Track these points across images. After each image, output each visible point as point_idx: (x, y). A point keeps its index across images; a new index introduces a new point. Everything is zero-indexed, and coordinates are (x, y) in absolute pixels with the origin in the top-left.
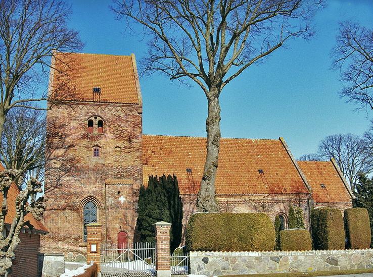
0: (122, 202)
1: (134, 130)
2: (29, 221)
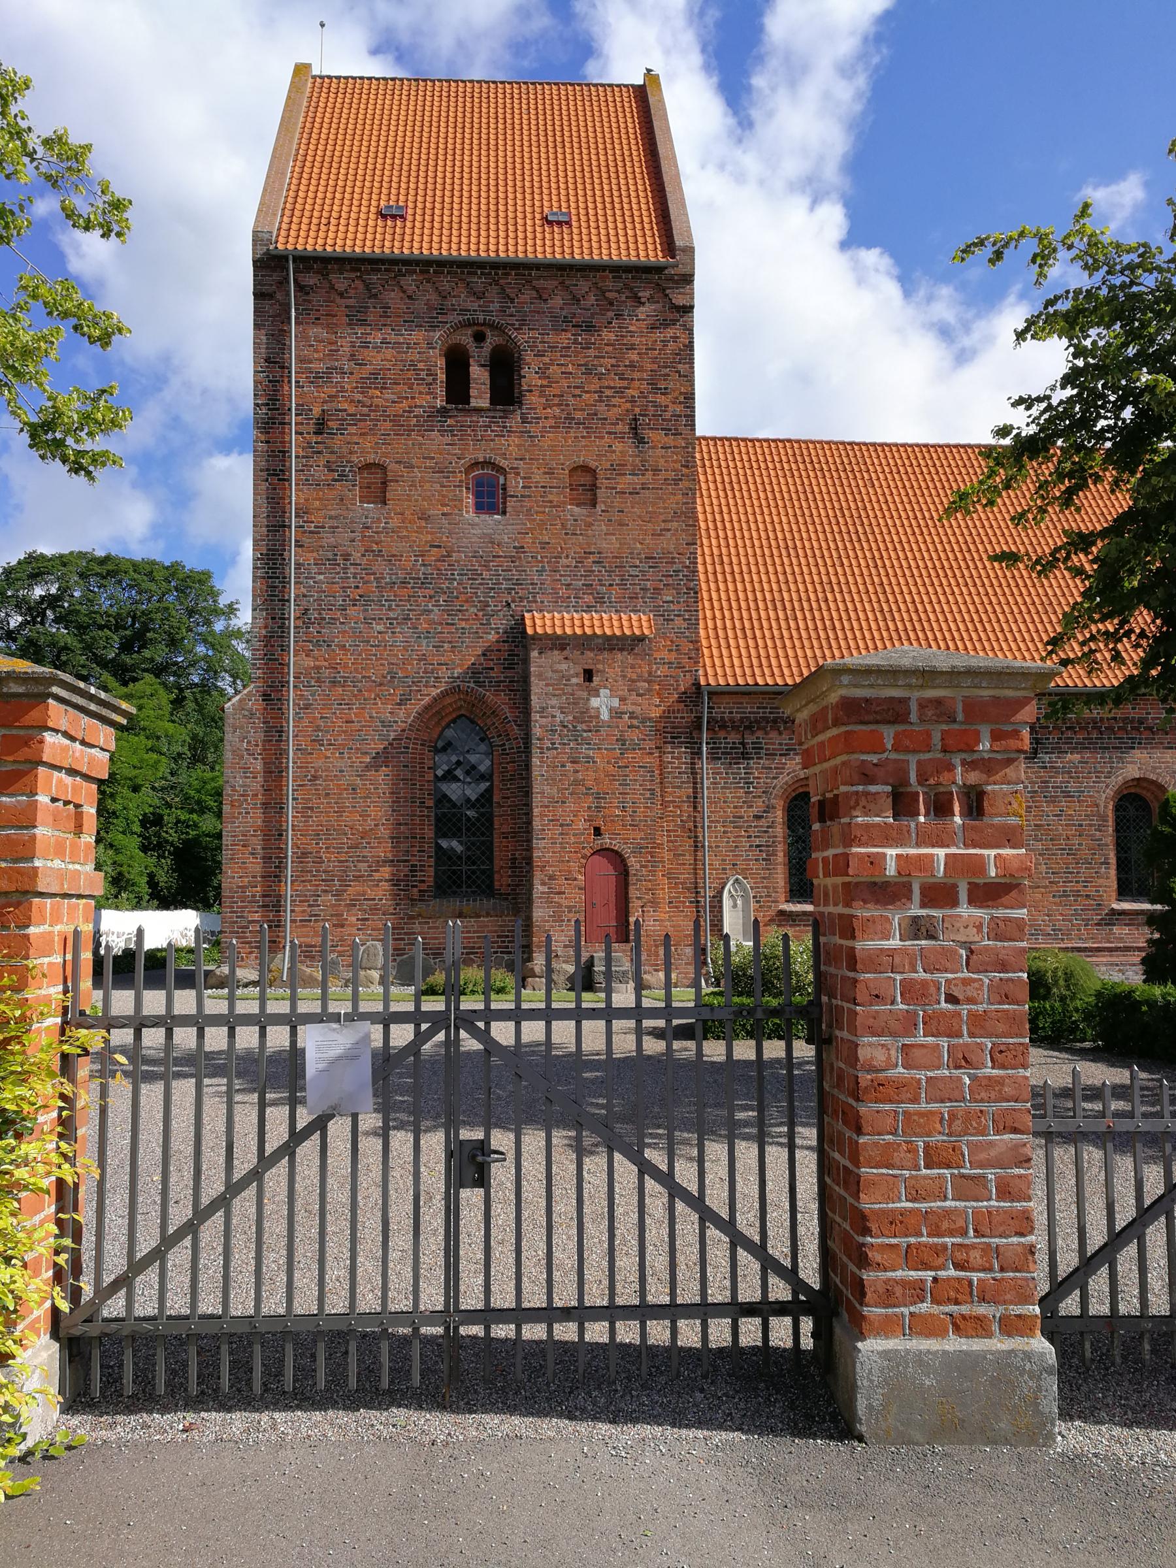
0: (605, 716)
1: (656, 389)
2: (301, 70)
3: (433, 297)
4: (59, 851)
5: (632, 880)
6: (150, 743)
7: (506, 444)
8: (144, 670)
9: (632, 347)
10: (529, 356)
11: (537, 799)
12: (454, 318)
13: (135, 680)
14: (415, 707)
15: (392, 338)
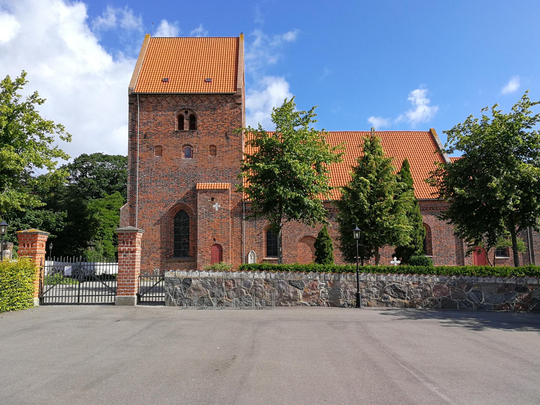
3: (174, 103)
4: (40, 249)
5: (223, 252)
6: (116, 213)
7: (193, 140)
8: (117, 190)
9: (226, 114)
10: (199, 117)
11: (198, 231)
12: (180, 108)
13: (113, 193)
14: (168, 208)
15: (164, 113)
